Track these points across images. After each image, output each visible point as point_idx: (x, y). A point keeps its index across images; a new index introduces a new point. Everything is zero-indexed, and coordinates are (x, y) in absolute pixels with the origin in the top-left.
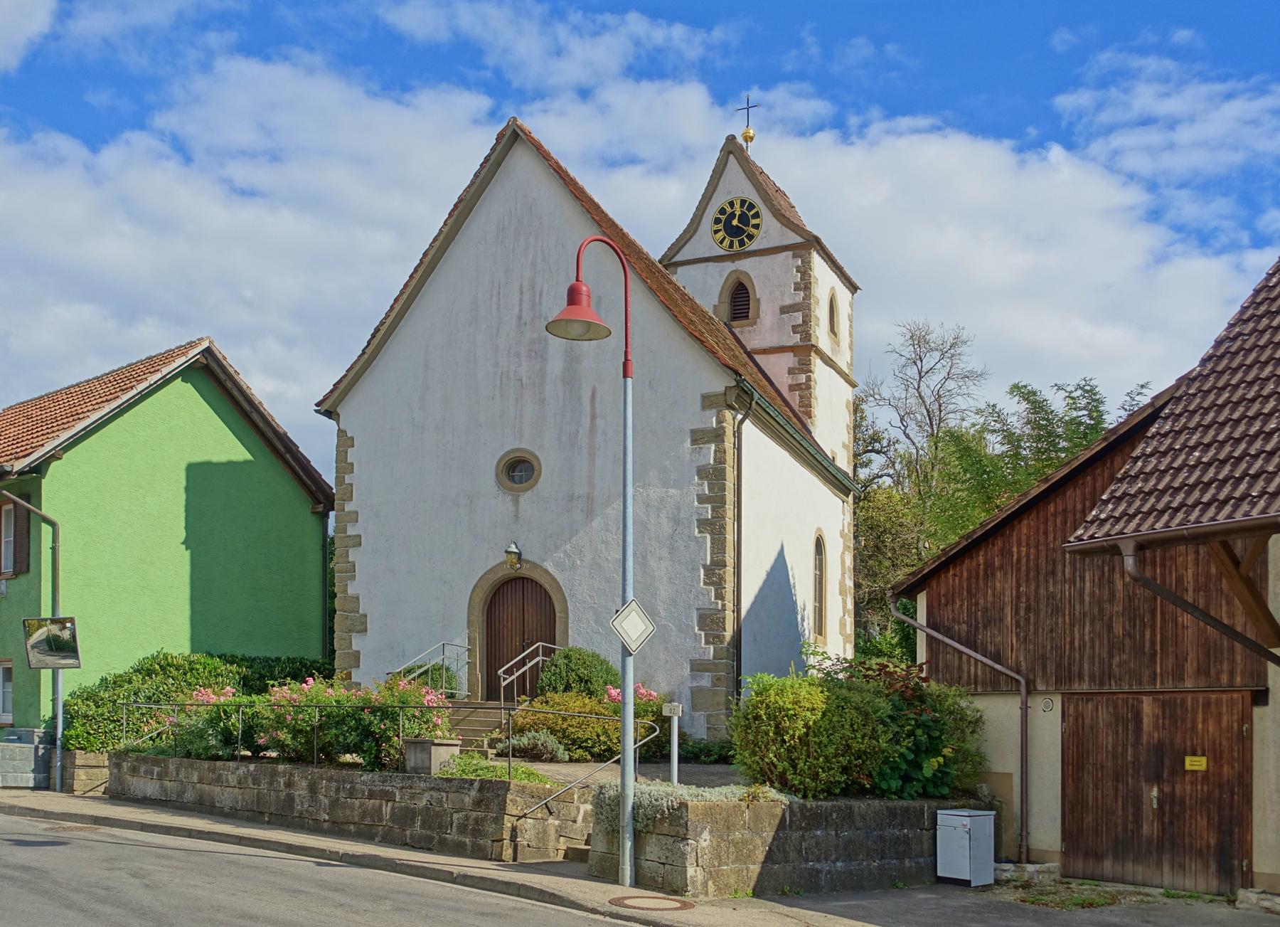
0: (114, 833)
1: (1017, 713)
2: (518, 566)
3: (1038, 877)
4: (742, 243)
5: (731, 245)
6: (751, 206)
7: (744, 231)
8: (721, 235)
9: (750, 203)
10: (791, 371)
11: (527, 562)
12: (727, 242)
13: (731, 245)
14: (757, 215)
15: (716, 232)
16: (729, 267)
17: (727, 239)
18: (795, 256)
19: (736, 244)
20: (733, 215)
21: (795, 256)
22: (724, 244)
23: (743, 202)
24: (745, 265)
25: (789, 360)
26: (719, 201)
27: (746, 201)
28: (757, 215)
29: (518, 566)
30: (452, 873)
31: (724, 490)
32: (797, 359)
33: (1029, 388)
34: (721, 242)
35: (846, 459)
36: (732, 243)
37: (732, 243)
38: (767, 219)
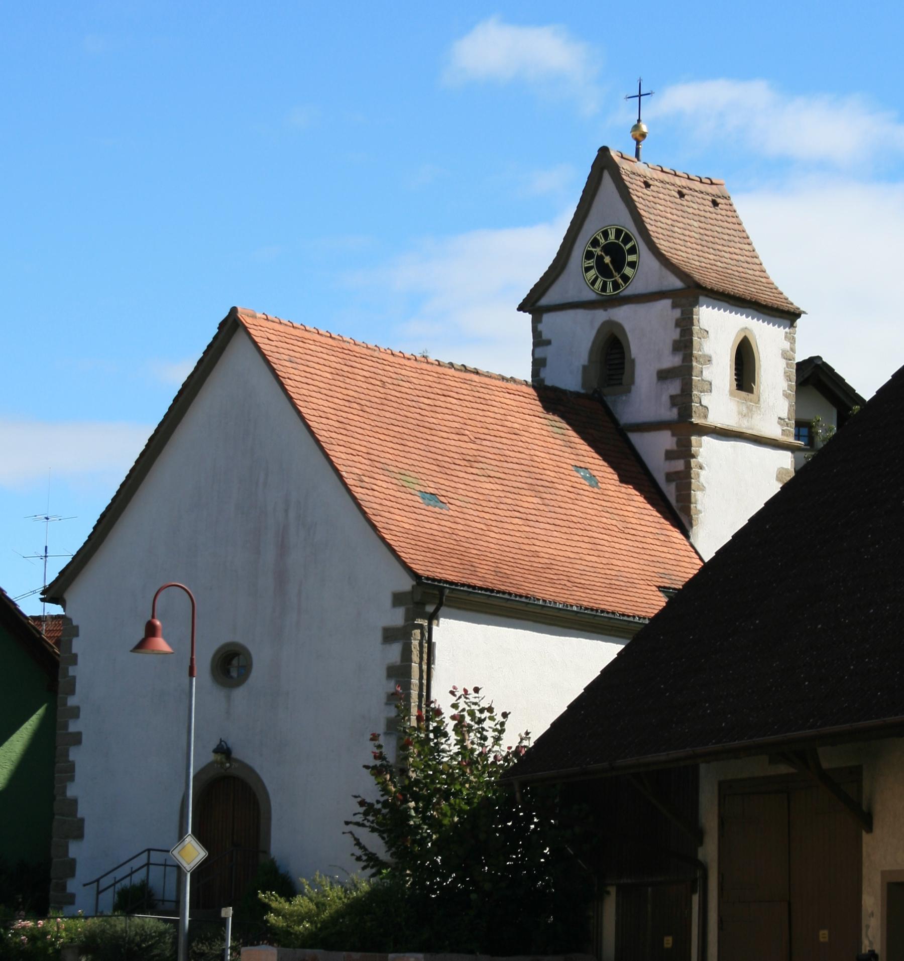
0: (493, 603)
1: (155, 852)
2: (228, 765)
3: (322, 908)
4: (616, 286)
5: (604, 288)
6: (628, 239)
7: (611, 276)
8: (592, 273)
9: (626, 234)
10: (670, 455)
11: (237, 761)
12: (599, 284)
13: (604, 288)
14: (633, 251)
15: (588, 269)
16: (601, 316)
17: (599, 280)
18: (674, 306)
19: (610, 286)
20: (600, 259)
21: (674, 306)
22: (596, 286)
23: (618, 232)
24: (622, 315)
25: (665, 440)
26: (591, 229)
27: (622, 231)
28: (633, 251)
29: (228, 765)
30: (189, 920)
31: (409, 689)
32: (675, 439)
33: (381, 729)
34: (593, 283)
35: (627, 612)
36: (605, 284)
37: (605, 284)
38: (645, 256)
